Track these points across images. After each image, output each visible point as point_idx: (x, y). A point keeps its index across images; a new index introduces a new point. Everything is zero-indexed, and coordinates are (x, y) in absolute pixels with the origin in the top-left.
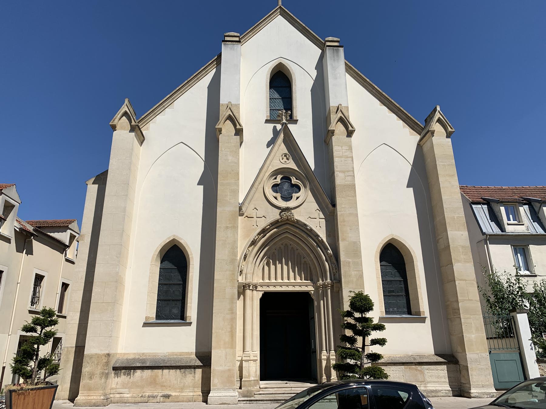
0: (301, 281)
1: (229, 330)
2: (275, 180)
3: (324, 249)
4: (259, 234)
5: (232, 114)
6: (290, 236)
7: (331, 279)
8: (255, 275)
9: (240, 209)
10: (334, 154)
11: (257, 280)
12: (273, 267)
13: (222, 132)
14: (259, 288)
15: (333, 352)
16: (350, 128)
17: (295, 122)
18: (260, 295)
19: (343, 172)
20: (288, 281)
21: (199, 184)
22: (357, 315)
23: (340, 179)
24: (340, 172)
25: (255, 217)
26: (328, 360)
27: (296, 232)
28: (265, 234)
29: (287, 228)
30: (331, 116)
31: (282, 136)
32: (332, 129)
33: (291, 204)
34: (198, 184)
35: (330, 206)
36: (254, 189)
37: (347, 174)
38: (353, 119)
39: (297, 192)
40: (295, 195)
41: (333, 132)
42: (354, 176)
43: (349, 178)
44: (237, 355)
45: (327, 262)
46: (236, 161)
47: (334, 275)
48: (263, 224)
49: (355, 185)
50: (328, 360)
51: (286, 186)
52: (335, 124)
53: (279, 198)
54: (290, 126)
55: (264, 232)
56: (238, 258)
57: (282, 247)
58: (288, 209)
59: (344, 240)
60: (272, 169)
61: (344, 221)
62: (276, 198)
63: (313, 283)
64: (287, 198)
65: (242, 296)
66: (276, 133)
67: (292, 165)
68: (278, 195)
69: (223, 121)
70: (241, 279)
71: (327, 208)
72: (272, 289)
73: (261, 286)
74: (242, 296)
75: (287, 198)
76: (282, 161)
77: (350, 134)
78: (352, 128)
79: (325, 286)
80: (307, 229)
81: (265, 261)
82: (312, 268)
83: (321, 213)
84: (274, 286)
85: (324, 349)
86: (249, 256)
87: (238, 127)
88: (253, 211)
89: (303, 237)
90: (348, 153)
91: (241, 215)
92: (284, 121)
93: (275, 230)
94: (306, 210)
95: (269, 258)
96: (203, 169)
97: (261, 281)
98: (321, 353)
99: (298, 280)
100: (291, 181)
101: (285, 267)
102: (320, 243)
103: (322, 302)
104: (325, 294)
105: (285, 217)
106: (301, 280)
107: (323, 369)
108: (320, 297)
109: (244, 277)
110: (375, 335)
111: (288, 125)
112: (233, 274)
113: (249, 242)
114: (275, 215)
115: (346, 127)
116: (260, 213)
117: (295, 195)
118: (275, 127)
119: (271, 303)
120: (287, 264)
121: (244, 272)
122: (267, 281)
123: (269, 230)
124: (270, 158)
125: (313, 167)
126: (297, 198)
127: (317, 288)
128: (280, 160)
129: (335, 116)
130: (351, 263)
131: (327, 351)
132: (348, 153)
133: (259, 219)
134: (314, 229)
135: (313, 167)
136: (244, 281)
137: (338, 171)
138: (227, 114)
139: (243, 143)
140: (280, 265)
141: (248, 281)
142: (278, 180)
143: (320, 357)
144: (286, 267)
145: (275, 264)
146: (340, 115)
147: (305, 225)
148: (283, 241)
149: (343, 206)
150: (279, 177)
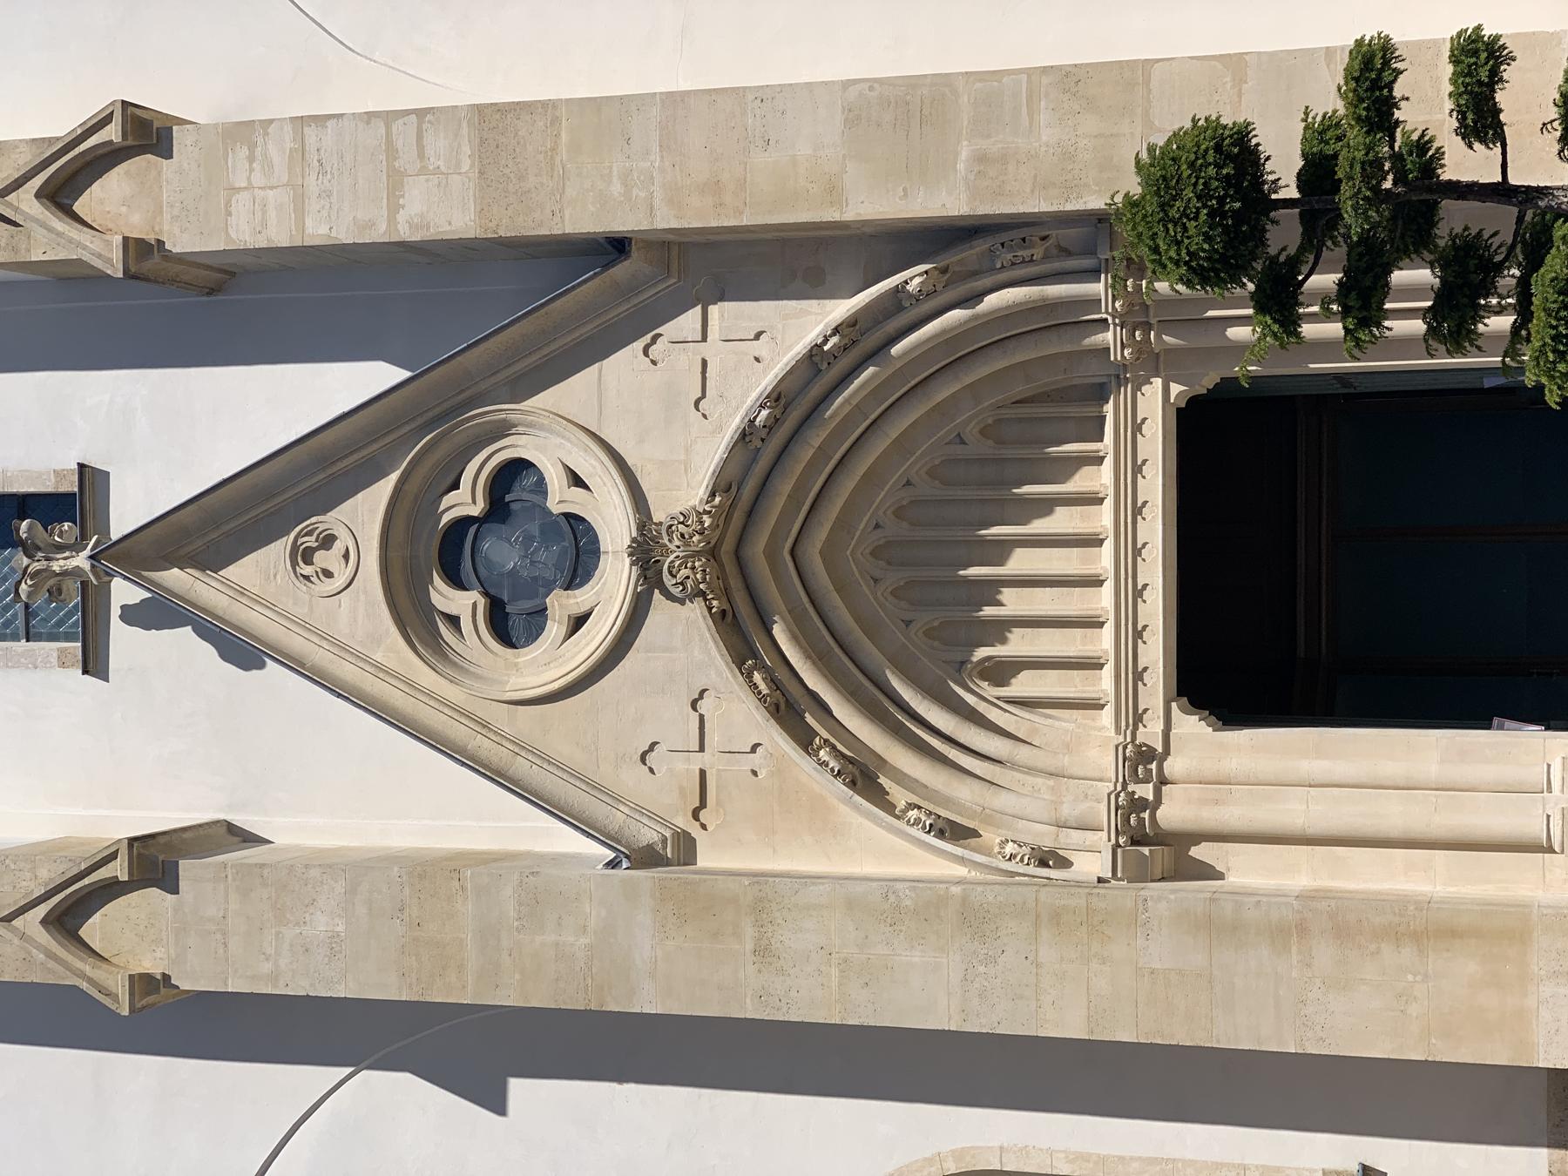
0: (1108, 462)
1: (1407, 953)
2: (466, 624)
4: (805, 740)
5: (42, 910)
7: (1093, 274)
8: (1065, 762)
9: (647, 858)
10: (284, 242)
11: (1095, 746)
12: (1019, 644)
13: (157, 971)
14: (1151, 733)
16: (112, 133)
17: (91, 479)
18: (1191, 726)
19: (396, 183)
20: (1108, 546)
21: (498, 1105)
22: (1284, 235)
23: (442, 209)
24: (394, 208)
25: (697, 762)
27: (795, 498)
29: (771, 555)
30: (37, 256)
31: (175, 578)
32: (117, 255)
33: (614, 527)
34: (500, 1108)
36: (522, 767)
37: (407, 157)
38: (53, 113)
39: (541, 487)
40: (560, 497)
41: (140, 250)
42: (421, 113)
43: (437, 144)
45: (979, 296)
46: (340, 887)
47: (1066, 252)
48: (739, 713)
49: (479, 109)
51: (502, 552)
52: (83, 236)
53: (579, 599)
54: (127, 513)
55: (789, 709)
56: (961, 871)
58: (645, 553)
59: (833, 191)
60: (393, 648)
61: (714, 187)
62: (579, 622)
63: (1120, 381)
64: (577, 550)
65: (1199, 852)
66: (158, 613)
67: (363, 515)
68: (561, 604)
69: (87, 967)
70: (1092, 859)
72: (1156, 653)
73: (1138, 719)
74: (1199, 852)
75: (577, 550)
76: (339, 581)
77: (146, 134)
78: (105, 121)
79: (1137, 316)
80: (772, 425)
81: (981, 695)
82: (1020, 389)
83: (669, 330)
84: (1138, 635)
86: (947, 802)
87: (118, 870)
88: (661, 771)
89: (822, 452)
90: (276, 150)
91: (686, 849)
92: (81, 561)
93: (778, 631)
94: (647, 428)
95: (960, 668)
96: (408, 1075)
97: (1107, 716)
99: (1101, 478)
100: (464, 523)
101: (1022, 562)
102: (862, 340)
105: (696, 572)
106: (1099, 460)
109: (1076, 837)
110: (1425, 105)
111: (117, 530)
112: (1056, 916)
113: (857, 808)
114: (683, 634)
115: (107, 159)
116: (677, 728)
117: (560, 497)
118: (131, 615)
119: (1264, 638)
120: (1000, 551)
121: (1046, 837)
122: (1104, 683)
123: (782, 674)
124: (320, 655)
125: (374, 377)
126: (577, 481)
127: (1151, 363)
128: (333, 590)
129: (39, 233)
132: (276, 150)
133: (713, 738)
134: (767, 379)
135: (374, 377)
136: (1102, 840)
137: (392, 220)
138: (43, 936)
139: (238, 819)
140: (1007, 594)
141: (1101, 812)
142: (463, 603)
144: (1019, 553)
145: (1000, 629)
146: (26, 202)
147: (746, 435)
148: (846, 581)
149: (616, 188)
150: (445, 597)
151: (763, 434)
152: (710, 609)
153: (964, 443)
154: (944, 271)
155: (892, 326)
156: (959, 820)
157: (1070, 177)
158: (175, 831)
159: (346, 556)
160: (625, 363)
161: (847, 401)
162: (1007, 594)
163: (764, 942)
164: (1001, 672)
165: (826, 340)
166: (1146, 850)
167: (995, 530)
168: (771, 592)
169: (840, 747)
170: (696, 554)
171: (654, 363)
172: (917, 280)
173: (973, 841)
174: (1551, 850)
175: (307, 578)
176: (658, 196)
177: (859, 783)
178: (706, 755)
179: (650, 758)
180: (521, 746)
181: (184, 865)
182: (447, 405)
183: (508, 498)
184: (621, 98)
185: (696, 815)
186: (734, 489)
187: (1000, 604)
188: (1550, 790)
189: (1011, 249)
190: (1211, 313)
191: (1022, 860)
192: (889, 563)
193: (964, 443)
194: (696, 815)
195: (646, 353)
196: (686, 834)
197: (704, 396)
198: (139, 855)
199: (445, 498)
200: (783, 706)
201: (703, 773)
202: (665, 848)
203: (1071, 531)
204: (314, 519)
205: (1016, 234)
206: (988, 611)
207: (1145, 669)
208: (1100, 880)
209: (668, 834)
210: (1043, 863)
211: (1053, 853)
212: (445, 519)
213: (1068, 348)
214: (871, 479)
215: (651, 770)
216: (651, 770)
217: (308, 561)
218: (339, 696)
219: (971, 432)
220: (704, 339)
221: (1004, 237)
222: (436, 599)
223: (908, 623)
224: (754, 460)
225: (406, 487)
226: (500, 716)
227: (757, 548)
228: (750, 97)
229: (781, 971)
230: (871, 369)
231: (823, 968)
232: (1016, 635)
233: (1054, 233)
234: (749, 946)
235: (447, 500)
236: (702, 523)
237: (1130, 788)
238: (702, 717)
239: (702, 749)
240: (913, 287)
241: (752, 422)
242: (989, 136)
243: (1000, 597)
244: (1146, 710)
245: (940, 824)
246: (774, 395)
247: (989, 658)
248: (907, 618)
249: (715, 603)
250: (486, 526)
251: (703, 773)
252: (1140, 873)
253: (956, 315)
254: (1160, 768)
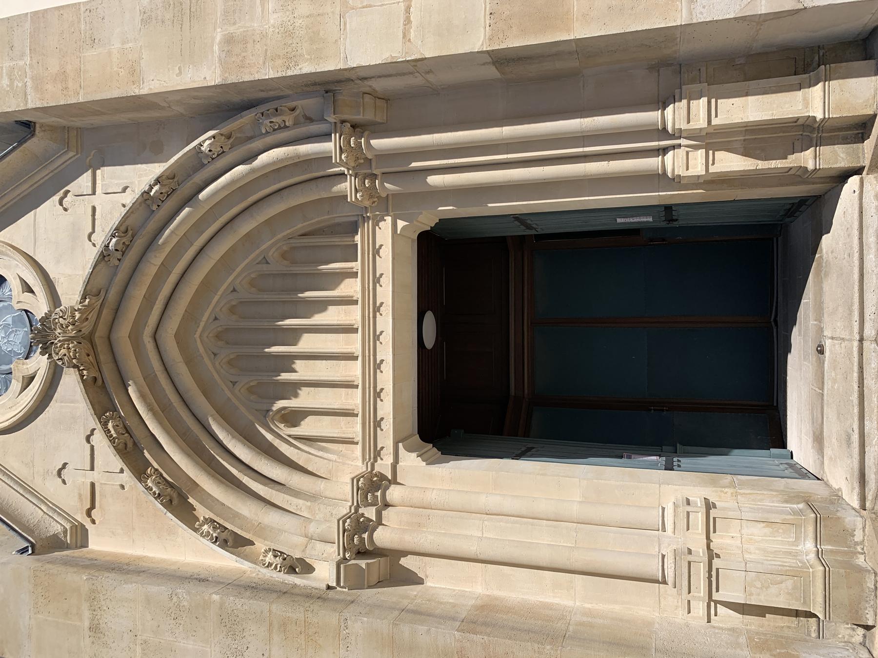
3: (199, 169)
4: (140, 470)
7: (325, 136)
12: (305, 399)
14: (384, 465)
15: (673, 116)
18: (410, 461)
26: (713, 139)
28: (143, 442)
29: (135, 337)
35: (35, 145)
44: (680, 616)
45: (255, 156)
47: (310, 120)
50: (713, 139)
55: (133, 450)
59: (134, 72)
61: (62, 76)
63: (365, 219)
70: (324, 573)
71: (42, 160)
79: (366, 167)
80: (124, 249)
82: (301, 226)
85: (653, 163)
86: (235, 516)
91: (81, 536)
93: (131, 390)
95: (264, 415)
98: (676, 182)
99: (351, 288)
101: (308, 343)
103: (434, 180)
104: (397, 165)
107: (761, 165)
108: (413, 187)
116: (78, 456)
120: (293, 336)
123: (132, 423)
127: (386, 205)
130: (232, 29)
131: (664, 151)
136: (333, 552)
140: (299, 364)
141: (332, 530)
143: (695, 182)
145: (292, 389)
151: (118, 255)
152: (82, 376)
153: (267, 263)
154: (229, 137)
155: (199, 178)
156: (239, 532)
157: (290, 49)
160: (49, 207)
161: (172, 232)
162: (299, 364)
163: (96, 622)
164: (293, 417)
165: (151, 188)
166: (363, 563)
167: (288, 322)
168: (130, 364)
169: (165, 475)
171: (66, 210)
172: (208, 142)
173: (248, 548)
174: (664, 582)
176: (29, 84)
177: (175, 502)
179: (64, 472)
184: (8, 19)
185: (89, 513)
186: (103, 293)
187: (295, 371)
188: (664, 530)
189: (268, 116)
190: (414, 164)
191: (276, 568)
193: (267, 263)
194: (89, 513)
195: (61, 204)
196: (83, 526)
197: (93, 231)
201: (93, 485)
202: (66, 537)
203: (335, 322)
205: (271, 105)
206: (285, 376)
207: (382, 419)
208: (329, 588)
209: (68, 526)
210: (292, 570)
211: (301, 561)
213: (324, 195)
214: (207, 286)
215: (64, 482)
216: (64, 482)
220: (94, 193)
221: (262, 108)
223: (234, 383)
224: (115, 274)
227: (123, 331)
228: (83, 9)
229: (105, 644)
230: (187, 210)
231: (131, 645)
232: (304, 392)
233: (298, 103)
234: (87, 624)
236: (73, 317)
237: (361, 511)
238: (92, 448)
239: (92, 469)
240: (205, 147)
241: (107, 246)
242: (234, 24)
243: (294, 366)
244: (382, 448)
245: (224, 535)
247: (284, 408)
249: (85, 372)
251: (93, 485)
252: (359, 582)
253: (240, 169)
254: (384, 495)
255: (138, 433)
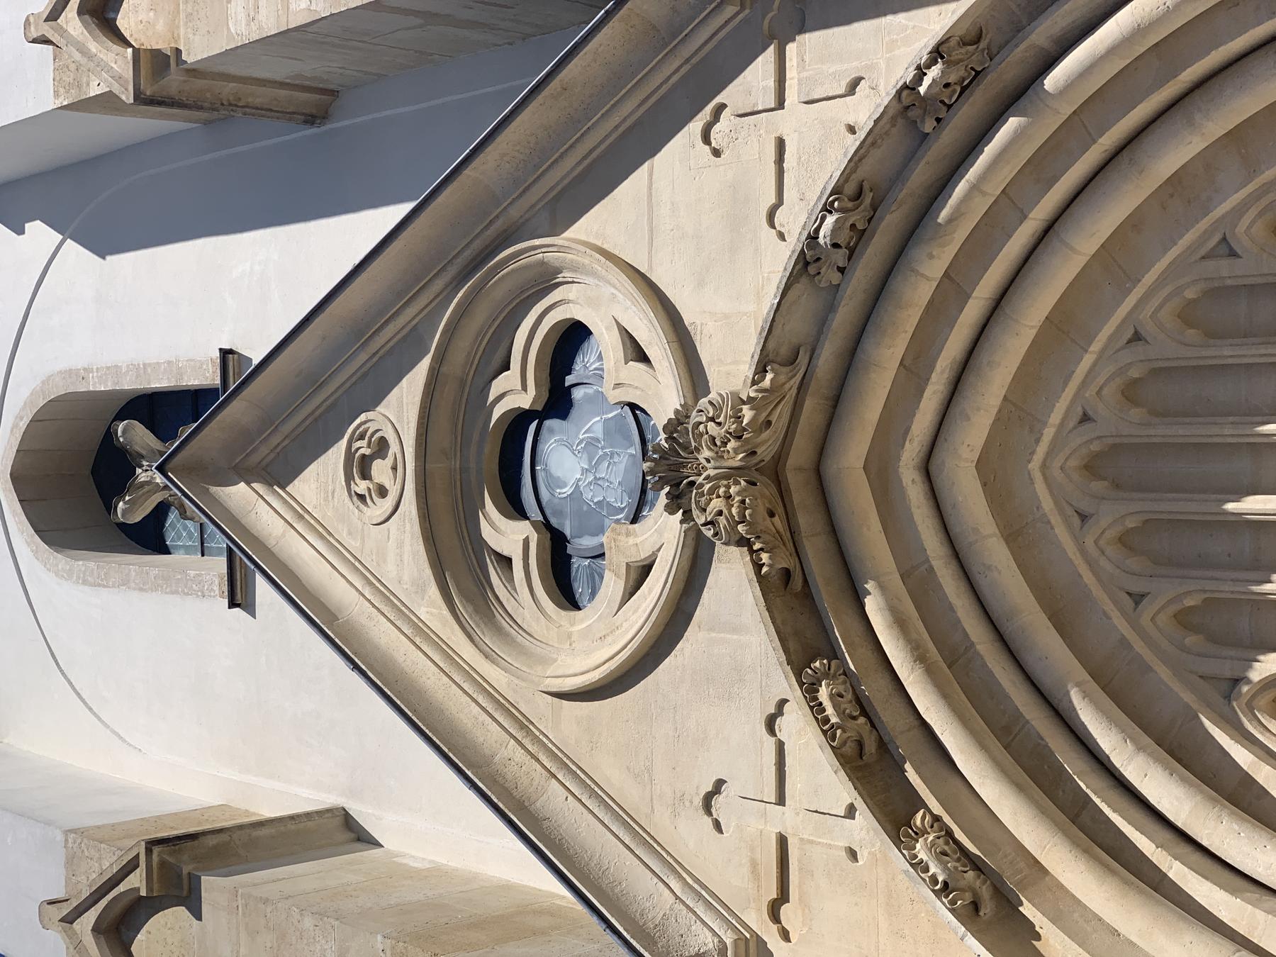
4: (897, 815)
5: (91, 917)
6: (972, 434)
28: (905, 742)
29: (880, 471)
36: (557, 802)
55: (879, 761)
57: (1114, 516)
80: (853, 242)
83: (732, 95)
89: (953, 288)
93: (874, 607)
100: (519, 421)
116: (749, 770)
123: (874, 689)
147: (807, 263)
151: (840, 257)
152: (758, 566)
153: (1233, 254)
158: (292, 818)
159: (394, 468)
161: (975, 188)
165: (921, 73)
170: (732, 474)
171: (717, 153)
175: (361, 497)
178: (787, 810)
179: (718, 802)
180: (564, 764)
181: (207, 882)
182: (478, 245)
183: (569, 380)
186: (803, 359)
192: (1117, 486)
195: (706, 139)
198: (162, 864)
199: (495, 383)
200: (871, 747)
201: (782, 842)
204: (363, 417)
209: (729, 939)
212: (497, 412)
214: (1063, 329)
215: (718, 826)
216: (718, 826)
217: (365, 475)
218: (356, 667)
219: (1248, 231)
220: (780, 104)
222: (486, 532)
223: (1138, 598)
224: (831, 308)
225: (444, 369)
226: (541, 710)
235: (497, 386)
236: (739, 418)
238: (780, 747)
241: (813, 237)
246: (850, 189)
248: (1137, 587)
249: (765, 557)
250: (547, 423)
251: (782, 842)
255: (891, 717)
